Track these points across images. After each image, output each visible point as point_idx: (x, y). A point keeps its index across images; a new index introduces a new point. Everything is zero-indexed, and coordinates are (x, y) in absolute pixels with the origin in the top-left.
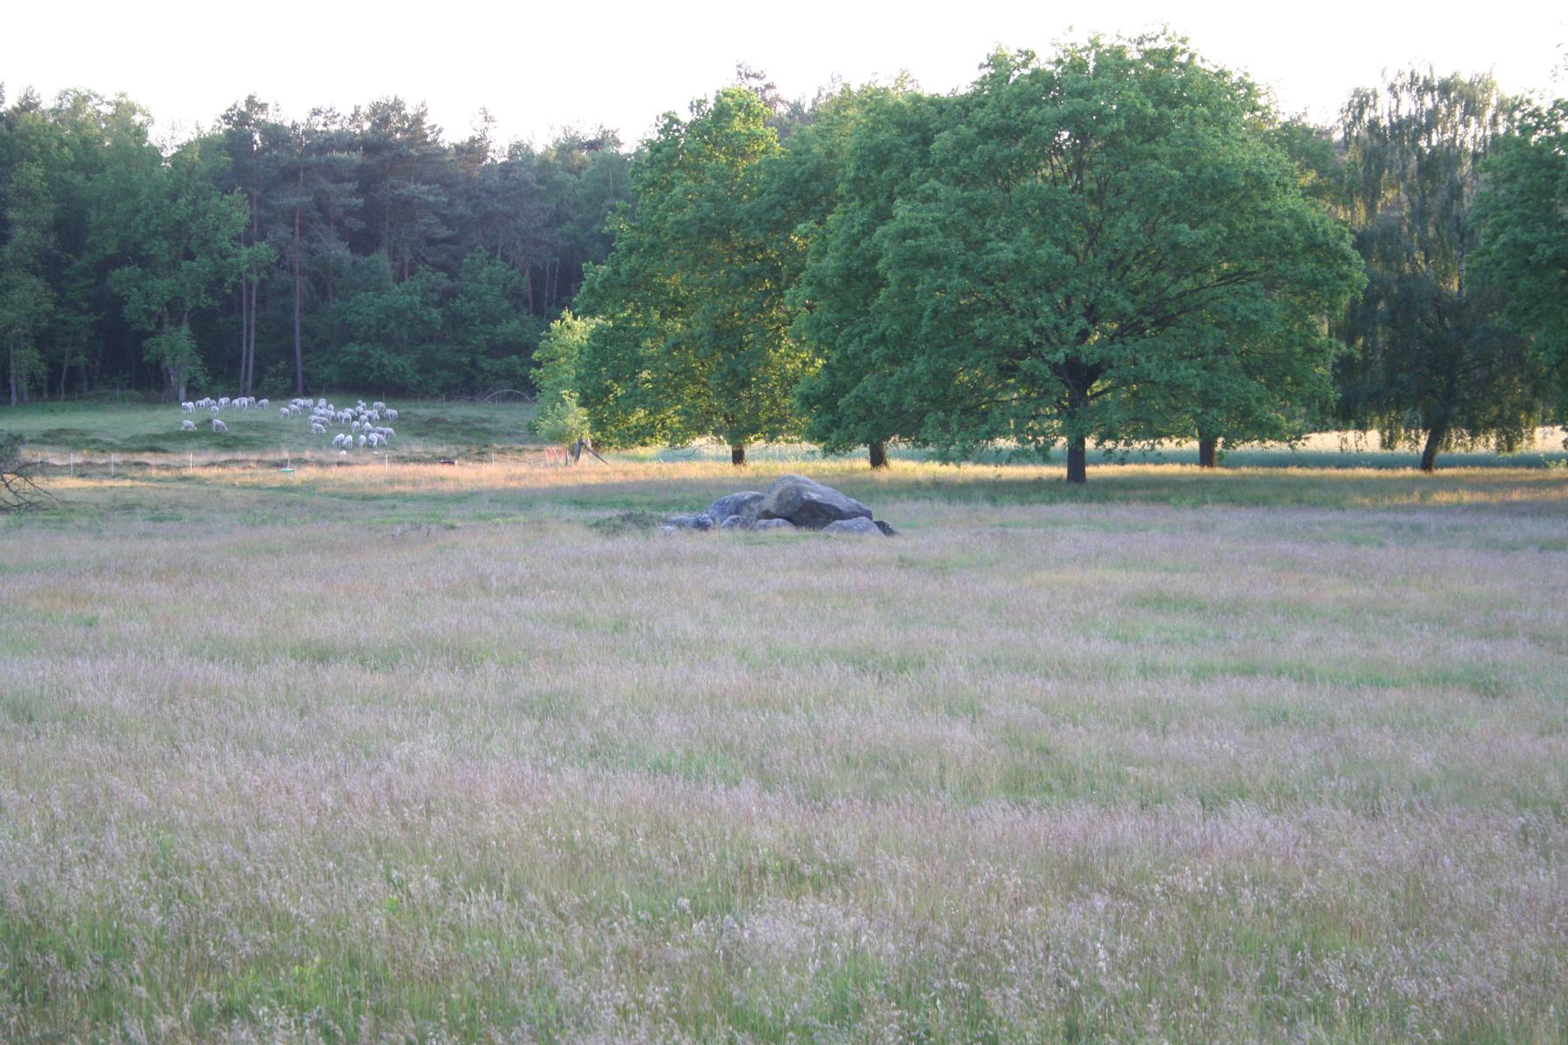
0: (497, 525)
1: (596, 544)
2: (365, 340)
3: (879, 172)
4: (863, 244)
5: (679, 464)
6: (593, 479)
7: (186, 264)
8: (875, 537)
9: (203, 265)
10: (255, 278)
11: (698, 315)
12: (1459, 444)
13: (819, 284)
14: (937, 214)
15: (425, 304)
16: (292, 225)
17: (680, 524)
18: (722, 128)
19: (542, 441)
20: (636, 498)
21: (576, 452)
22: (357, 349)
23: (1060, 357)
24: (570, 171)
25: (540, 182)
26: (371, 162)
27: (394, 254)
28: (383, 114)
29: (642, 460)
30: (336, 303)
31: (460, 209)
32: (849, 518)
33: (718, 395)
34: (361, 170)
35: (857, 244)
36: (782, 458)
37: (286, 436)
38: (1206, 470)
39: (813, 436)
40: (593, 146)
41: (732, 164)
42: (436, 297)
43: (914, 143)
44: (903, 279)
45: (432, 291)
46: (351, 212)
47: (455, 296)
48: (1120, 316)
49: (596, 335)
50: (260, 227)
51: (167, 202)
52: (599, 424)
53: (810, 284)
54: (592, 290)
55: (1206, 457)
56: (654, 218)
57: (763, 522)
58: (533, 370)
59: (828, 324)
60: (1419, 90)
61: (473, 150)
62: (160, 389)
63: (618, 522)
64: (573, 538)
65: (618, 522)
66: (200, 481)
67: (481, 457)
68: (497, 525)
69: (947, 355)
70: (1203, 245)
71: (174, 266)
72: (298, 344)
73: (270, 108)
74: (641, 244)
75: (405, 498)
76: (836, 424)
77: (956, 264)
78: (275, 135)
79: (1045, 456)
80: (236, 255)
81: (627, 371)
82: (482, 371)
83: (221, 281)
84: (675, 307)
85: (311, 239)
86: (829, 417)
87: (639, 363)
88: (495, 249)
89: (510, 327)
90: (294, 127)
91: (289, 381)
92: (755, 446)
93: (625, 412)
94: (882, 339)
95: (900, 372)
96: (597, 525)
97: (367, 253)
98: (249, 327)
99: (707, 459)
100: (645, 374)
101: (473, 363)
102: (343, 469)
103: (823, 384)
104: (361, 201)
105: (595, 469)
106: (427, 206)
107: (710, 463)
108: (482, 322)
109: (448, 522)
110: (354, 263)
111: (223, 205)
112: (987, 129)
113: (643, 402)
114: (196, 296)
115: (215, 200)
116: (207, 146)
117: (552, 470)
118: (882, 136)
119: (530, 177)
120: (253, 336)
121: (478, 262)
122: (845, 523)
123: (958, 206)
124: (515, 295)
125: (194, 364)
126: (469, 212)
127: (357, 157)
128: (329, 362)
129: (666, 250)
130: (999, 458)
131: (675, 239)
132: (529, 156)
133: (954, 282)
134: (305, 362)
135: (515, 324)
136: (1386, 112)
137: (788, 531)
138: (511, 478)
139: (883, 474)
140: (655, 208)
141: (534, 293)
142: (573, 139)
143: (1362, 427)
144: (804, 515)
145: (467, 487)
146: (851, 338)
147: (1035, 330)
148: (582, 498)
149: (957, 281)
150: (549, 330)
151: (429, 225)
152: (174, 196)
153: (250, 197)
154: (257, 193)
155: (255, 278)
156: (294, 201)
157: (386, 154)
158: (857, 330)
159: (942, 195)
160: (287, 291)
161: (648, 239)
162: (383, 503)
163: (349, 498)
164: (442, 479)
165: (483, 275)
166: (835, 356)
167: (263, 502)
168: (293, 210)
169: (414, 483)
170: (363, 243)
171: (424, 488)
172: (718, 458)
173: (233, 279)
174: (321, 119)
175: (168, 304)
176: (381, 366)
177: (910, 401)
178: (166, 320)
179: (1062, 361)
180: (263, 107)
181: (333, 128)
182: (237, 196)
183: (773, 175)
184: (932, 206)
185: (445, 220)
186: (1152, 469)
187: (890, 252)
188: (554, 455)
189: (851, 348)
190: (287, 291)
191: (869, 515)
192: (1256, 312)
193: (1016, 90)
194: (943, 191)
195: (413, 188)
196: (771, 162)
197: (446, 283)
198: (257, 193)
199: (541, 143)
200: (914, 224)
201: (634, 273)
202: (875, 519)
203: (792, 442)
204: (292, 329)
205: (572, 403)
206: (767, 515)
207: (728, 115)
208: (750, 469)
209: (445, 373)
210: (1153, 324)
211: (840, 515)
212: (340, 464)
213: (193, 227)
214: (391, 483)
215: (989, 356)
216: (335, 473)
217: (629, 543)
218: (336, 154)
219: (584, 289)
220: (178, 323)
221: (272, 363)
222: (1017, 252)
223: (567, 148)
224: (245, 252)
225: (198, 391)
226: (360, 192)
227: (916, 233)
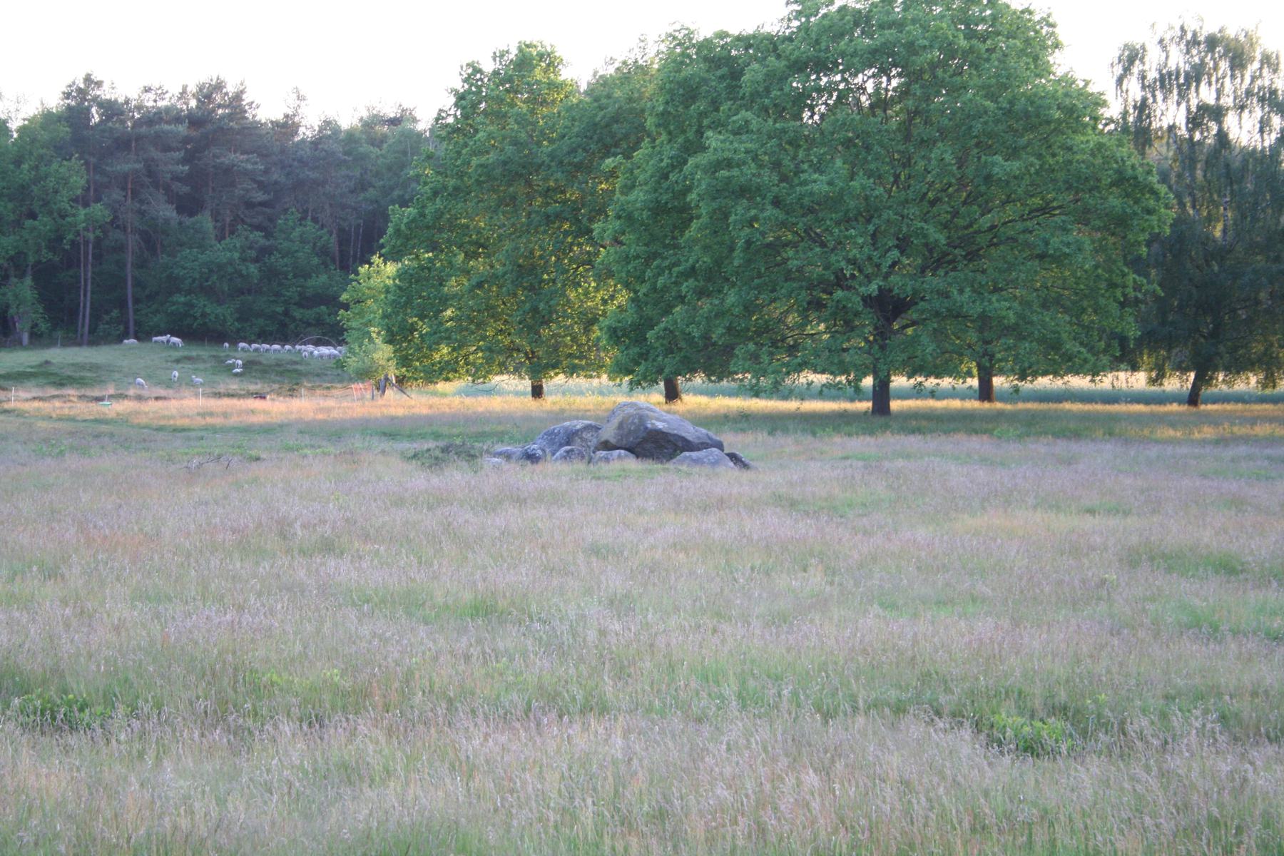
0: (305, 456)
1: (420, 480)
2: (189, 292)
3: (687, 107)
4: (673, 177)
5: (480, 398)
6: (400, 412)
7: (29, 223)
8: (729, 471)
9: (44, 224)
10: (91, 236)
11: (501, 256)
12: (1220, 383)
13: (628, 218)
14: (749, 145)
15: (244, 260)
16: (124, 189)
17: (508, 456)
18: (524, 76)
19: (351, 380)
20: (445, 430)
21: (381, 387)
22: (182, 299)
23: (873, 288)
24: (373, 145)
25: (346, 153)
26: (194, 133)
27: (216, 216)
28: (208, 93)
29: (444, 395)
30: (164, 259)
31: (275, 177)
32: (699, 450)
33: (520, 333)
34: (187, 140)
35: (666, 177)
36: (581, 393)
37: (117, 376)
38: (986, 405)
39: (620, 369)
40: (394, 122)
41: (533, 112)
42: (253, 254)
43: (722, 78)
44: (714, 211)
45: (251, 248)
46: (176, 178)
47: (271, 254)
48: (931, 248)
49: (401, 275)
50: (95, 190)
51: (12, 167)
52: (404, 361)
53: (619, 217)
54: (398, 231)
55: (986, 392)
56: (459, 162)
57: (603, 453)
58: (342, 311)
59: (638, 257)
60: (1188, 43)
61: (287, 127)
62: (6, 335)
63: (438, 453)
64: (389, 471)
65: (438, 453)
66: (20, 414)
67: (292, 393)
68: (305, 456)
69: (758, 287)
70: (1015, 177)
71: (18, 224)
72: (130, 296)
73: (106, 86)
74: (445, 188)
75: (214, 430)
76: (644, 356)
77: (770, 196)
78: (112, 110)
79: (858, 394)
80: (74, 215)
81: (431, 311)
82: (294, 319)
83: (60, 239)
84: (478, 247)
85: (141, 202)
86: (637, 350)
87: (445, 301)
88: (306, 212)
89: (320, 281)
90: (127, 102)
91: (122, 328)
92: (556, 381)
93: (430, 348)
94: (692, 272)
95: (705, 306)
96: (415, 456)
97: (191, 214)
98: (86, 280)
99: (508, 392)
100: (449, 313)
101: (286, 313)
102: (160, 403)
103: (630, 317)
104: (187, 168)
105: (396, 404)
106: (246, 173)
107: (511, 398)
108: (295, 276)
109: (254, 453)
110: (180, 223)
111: (61, 170)
112: (796, 62)
113: (448, 338)
114: (38, 251)
115: (55, 166)
116: (48, 119)
117: (359, 403)
118: (687, 72)
119: (338, 149)
120: (89, 288)
121: (291, 223)
122: (694, 454)
123: (770, 137)
124: (323, 252)
125: (36, 312)
126: (283, 179)
127: (182, 129)
128: (157, 311)
129: (469, 193)
130: (806, 393)
131: (479, 183)
132: (337, 131)
133: (767, 214)
134: (136, 311)
135: (323, 278)
136: (1154, 66)
137: (632, 463)
138: (321, 410)
139: (678, 406)
140: (459, 153)
141: (341, 251)
142: (375, 116)
143: (1135, 368)
144: (648, 446)
145: (277, 420)
146: (660, 271)
147: (849, 261)
148: (391, 431)
149: (770, 211)
150: (357, 274)
151: (248, 191)
152: (18, 162)
153: (87, 163)
154: (93, 160)
155: (91, 236)
156: (126, 167)
157: (209, 127)
158: (667, 263)
159: (754, 125)
160: (121, 248)
161: (452, 182)
162: (193, 434)
163: (160, 429)
164: (253, 412)
165: (296, 234)
166: (643, 289)
167: (72, 434)
168: (125, 176)
169: (225, 415)
170: (188, 206)
171: (233, 421)
172: (517, 394)
173: (70, 237)
174: (151, 96)
175: (11, 259)
176: (204, 315)
177: (717, 334)
178: (12, 272)
179: (875, 293)
180: (99, 84)
181: (161, 104)
182: (75, 162)
183: (574, 120)
184: (744, 137)
185: (262, 186)
186: (932, 403)
187: (703, 183)
188: (361, 389)
189: (661, 282)
190: (121, 248)
191: (720, 446)
192: (1068, 245)
193: (826, 22)
194: (755, 124)
195: (233, 157)
196: (570, 109)
197: (262, 242)
198: (93, 160)
199: (348, 120)
200: (727, 154)
201: (439, 215)
202: (726, 451)
203: (591, 377)
204: (125, 281)
205: (378, 341)
206: (607, 446)
207: (530, 64)
208: (551, 401)
209: (261, 321)
210: (965, 257)
211: (688, 446)
212: (157, 398)
213: (35, 188)
214: (203, 415)
215: (801, 287)
216: (152, 406)
217: (456, 476)
218: (166, 127)
219: (390, 230)
220: (21, 276)
221: (107, 312)
222: (830, 183)
223: (370, 124)
224: (82, 212)
225: (41, 335)
226: (184, 161)
227: (729, 164)
